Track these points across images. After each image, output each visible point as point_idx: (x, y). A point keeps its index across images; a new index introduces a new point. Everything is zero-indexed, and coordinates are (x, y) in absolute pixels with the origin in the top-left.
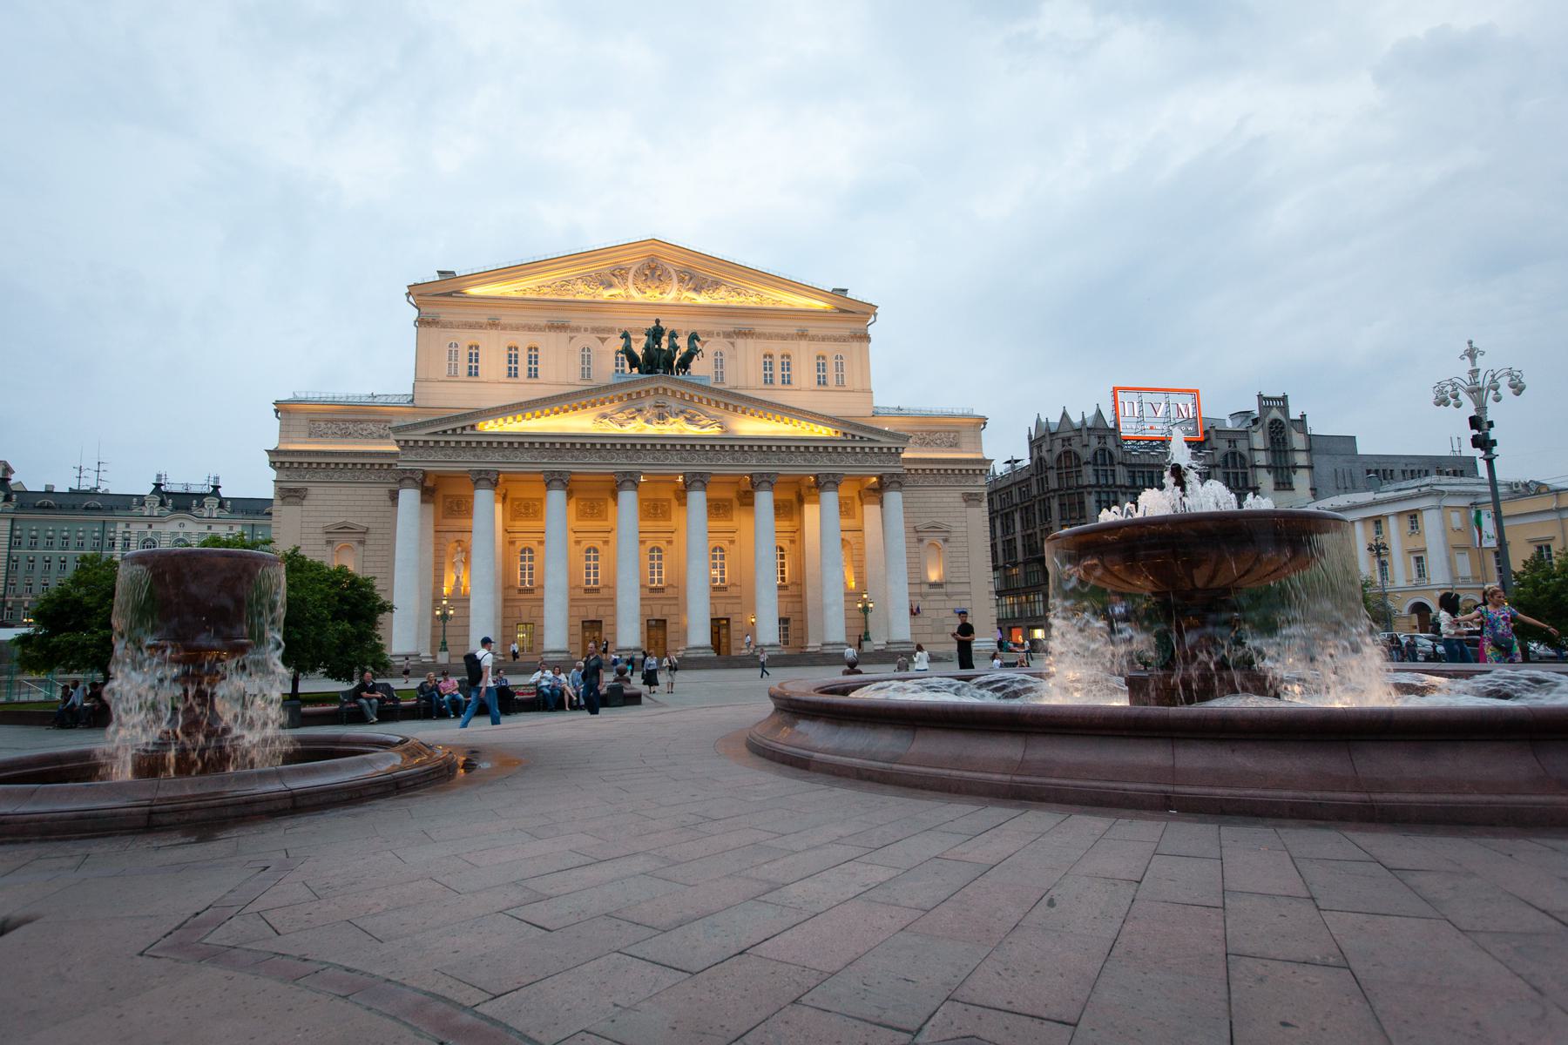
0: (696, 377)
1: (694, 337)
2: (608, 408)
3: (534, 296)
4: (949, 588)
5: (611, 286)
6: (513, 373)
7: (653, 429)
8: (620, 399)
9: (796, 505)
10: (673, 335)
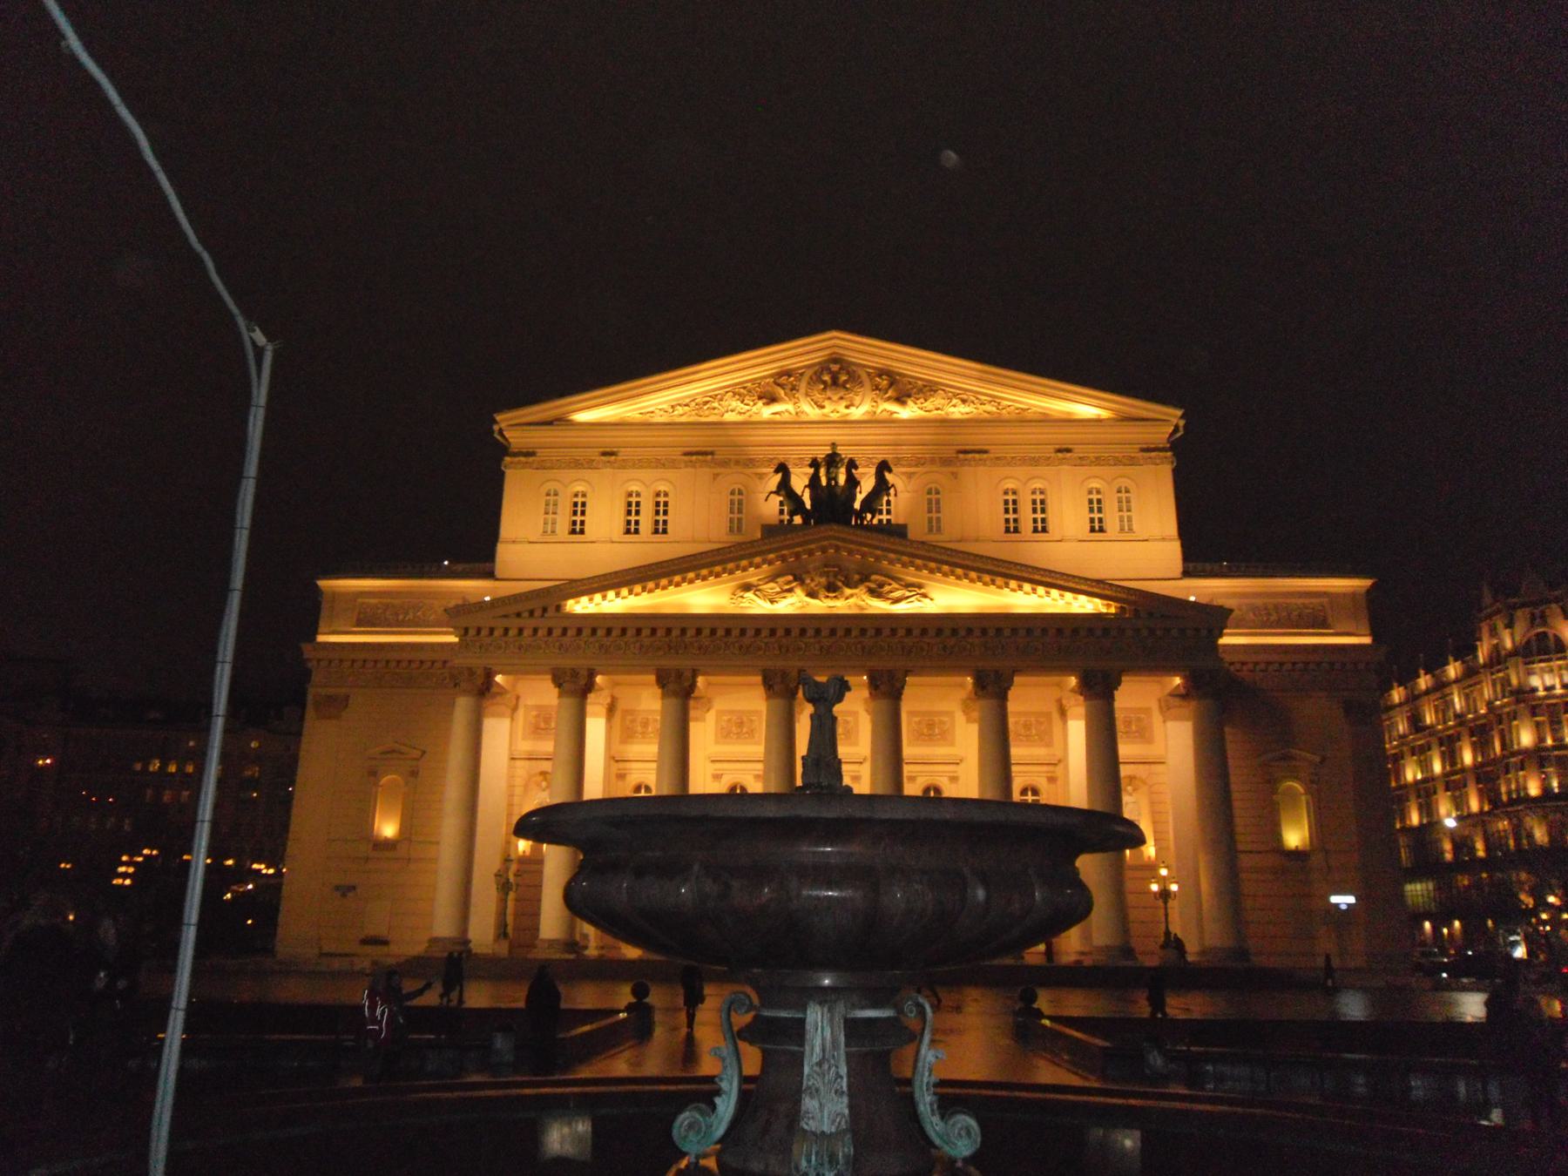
1: (883, 467)
2: (752, 576)
3: (691, 419)
5: (772, 399)
6: (631, 529)
7: (819, 606)
8: (783, 559)
9: (1056, 716)
10: (852, 465)
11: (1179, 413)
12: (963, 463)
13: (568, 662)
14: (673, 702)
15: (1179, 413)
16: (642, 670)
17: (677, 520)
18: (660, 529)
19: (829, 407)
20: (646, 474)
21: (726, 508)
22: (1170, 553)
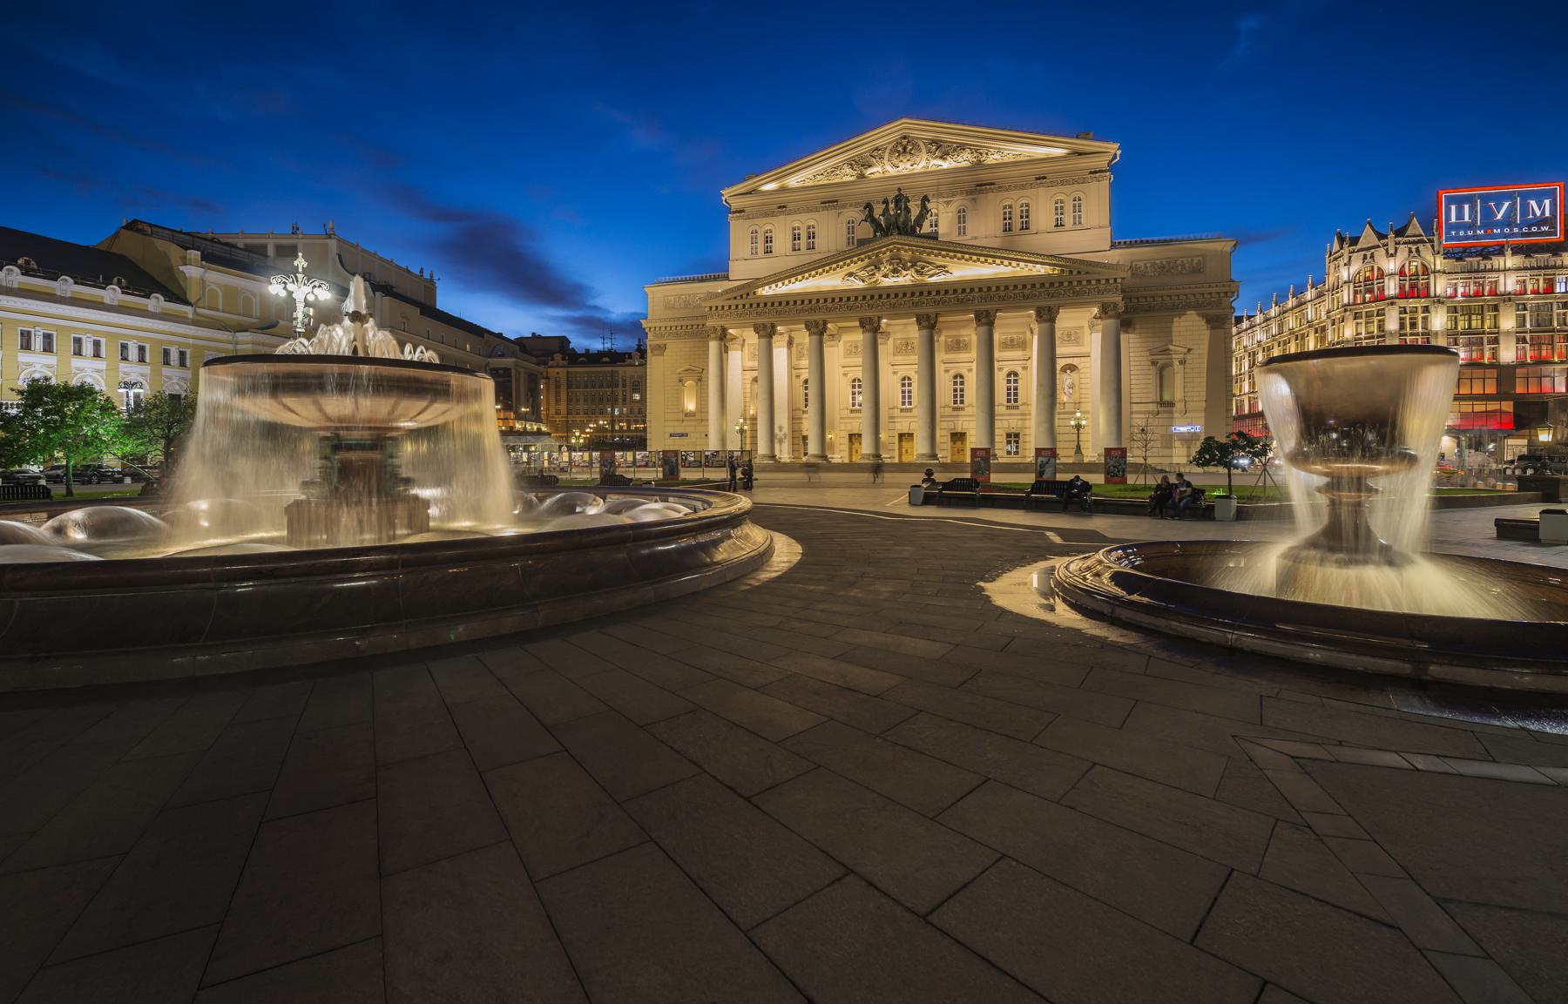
2: (853, 268)
11: (1117, 146)
12: (981, 192)
13: (760, 321)
14: (925, 332)
15: (1117, 146)
16: (908, 316)
17: (820, 242)
18: (811, 247)
19: (902, 166)
20: (802, 217)
21: (845, 231)
22: (1102, 237)
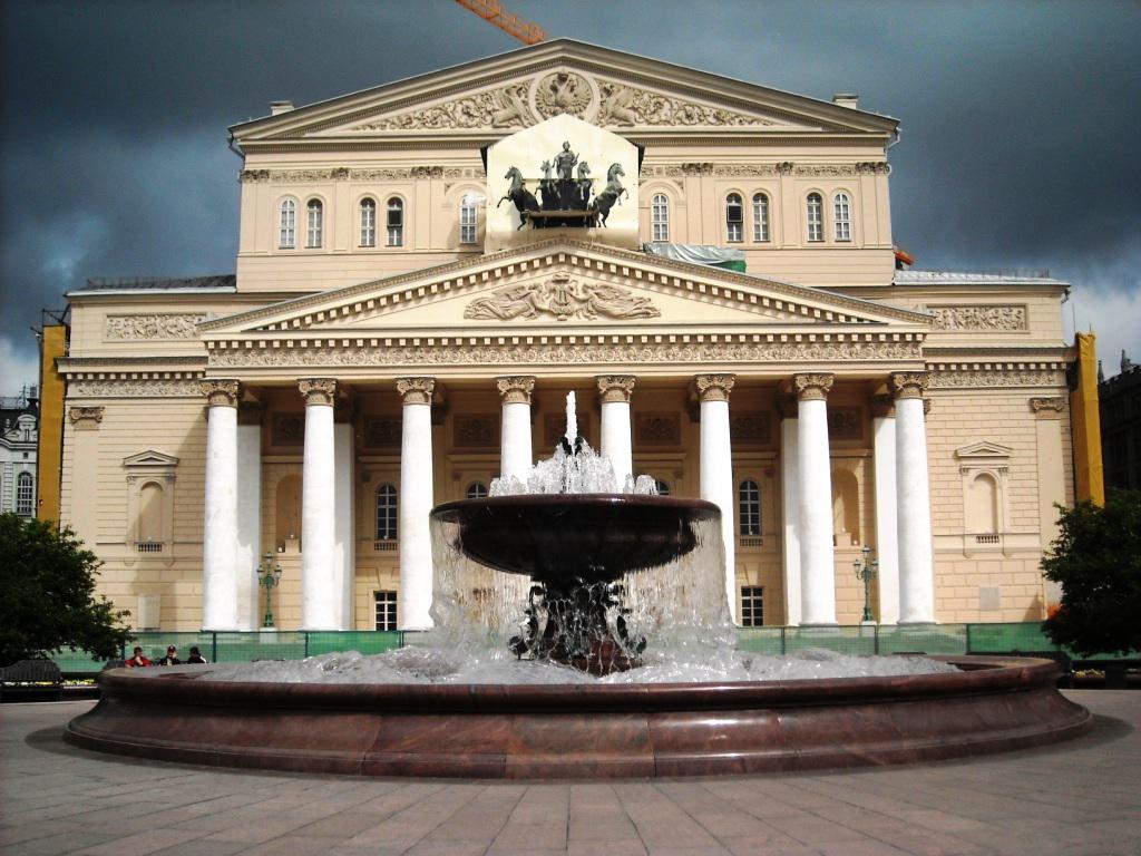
0: (476, 148)
4: (1009, 543)
